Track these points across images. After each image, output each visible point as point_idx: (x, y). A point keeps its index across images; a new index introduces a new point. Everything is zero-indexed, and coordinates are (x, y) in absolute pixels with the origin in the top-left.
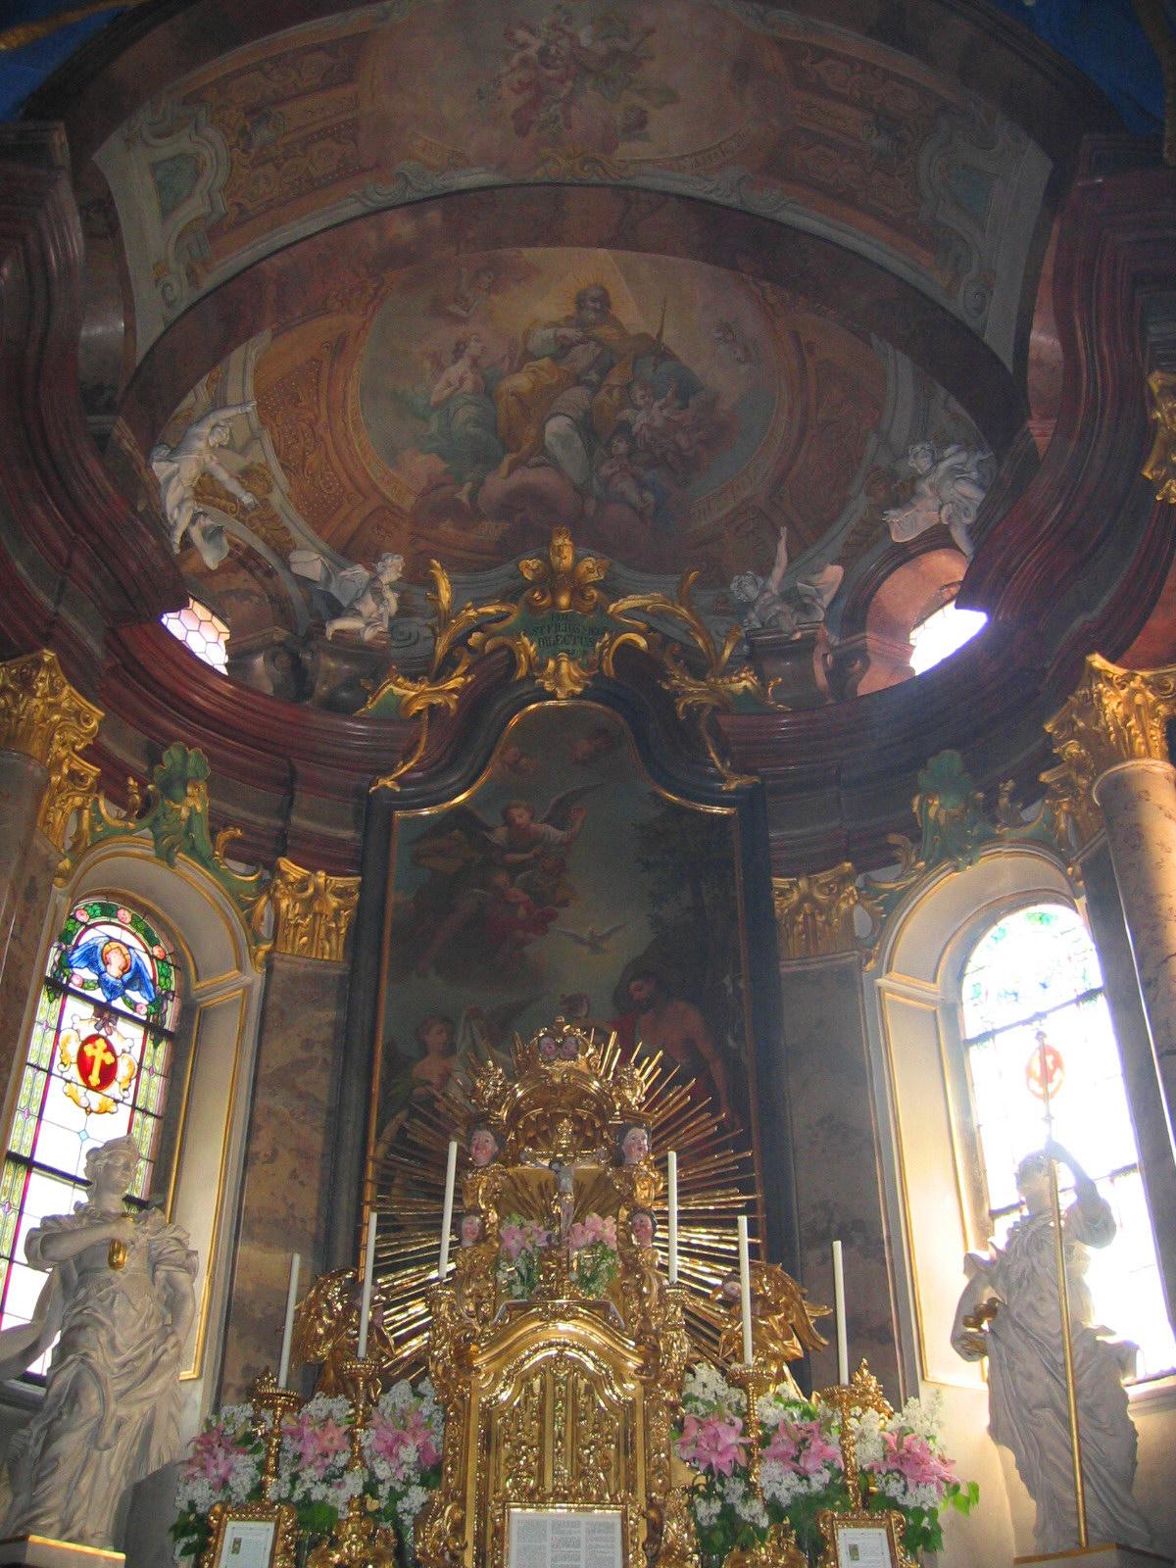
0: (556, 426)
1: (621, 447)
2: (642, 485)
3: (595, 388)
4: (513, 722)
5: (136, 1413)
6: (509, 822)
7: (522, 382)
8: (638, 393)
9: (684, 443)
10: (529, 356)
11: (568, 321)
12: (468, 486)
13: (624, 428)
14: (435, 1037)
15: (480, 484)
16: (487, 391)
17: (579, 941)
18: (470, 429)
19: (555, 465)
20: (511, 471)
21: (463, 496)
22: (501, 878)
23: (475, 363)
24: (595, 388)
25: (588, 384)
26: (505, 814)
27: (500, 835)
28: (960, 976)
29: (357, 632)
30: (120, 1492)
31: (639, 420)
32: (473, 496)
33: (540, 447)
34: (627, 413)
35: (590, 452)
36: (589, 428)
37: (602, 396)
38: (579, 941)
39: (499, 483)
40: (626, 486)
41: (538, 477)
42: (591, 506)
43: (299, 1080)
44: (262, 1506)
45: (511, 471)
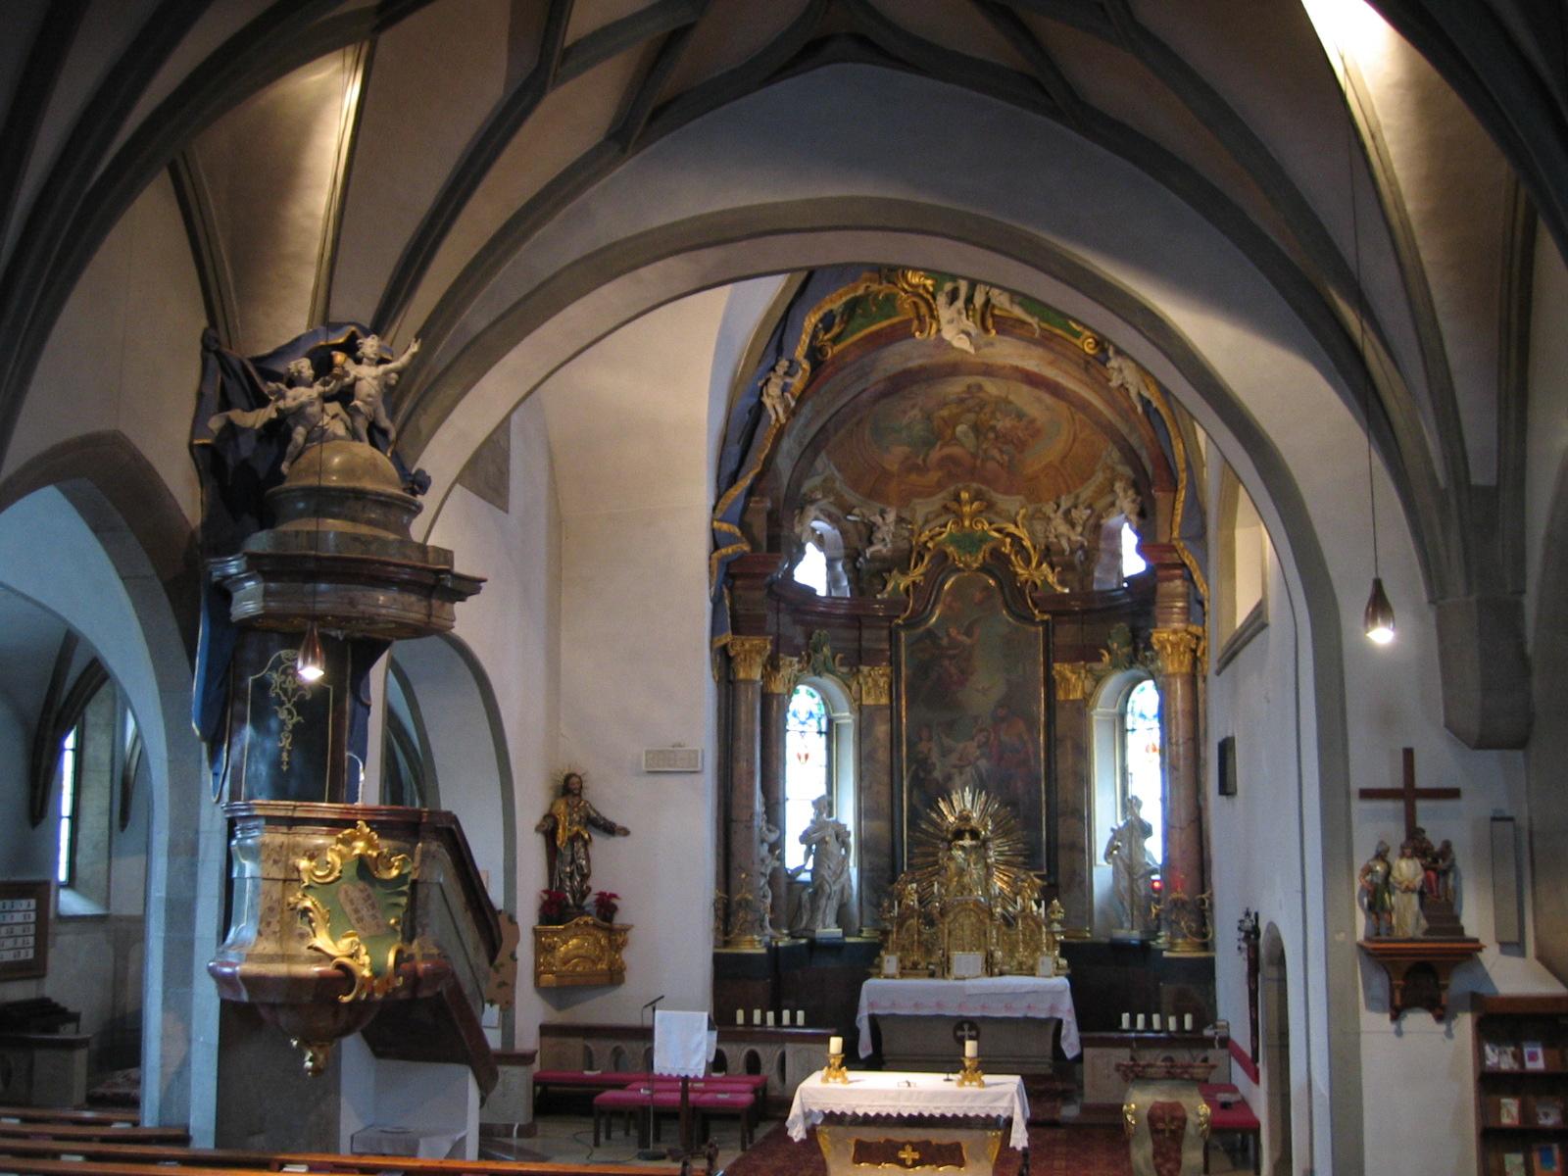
0: (961, 428)
1: (992, 435)
2: (1001, 451)
3: (978, 413)
4: (946, 587)
5: (836, 888)
6: (948, 635)
7: (945, 413)
8: (998, 415)
9: (1021, 435)
10: (946, 404)
11: (963, 392)
12: (921, 457)
13: (993, 428)
14: (925, 734)
15: (927, 455)
16: (928, 417)
17: (977, 690)
18: (922, 433)
19: (962, 446)
20: (941, 449)
21: (920, 461)
22: (946, 663)
23: (921, 409)
24: (978, 413)
25: (975, 412)
26: (947, 631)
27: (945, 642)
28: (1127, 702)
29: (880, 551)
30: (821, 911)
31: (1000, 425)
32: (924, 461)
33: (954, 437)
34: (993, 422)
35: (977, 438)
36: (977, 429)
37: (982, 415)
38: (977, 690)
39: (936, 454)
40: (995, 453)
41: (955, 450)
42: (979, 462)
43: (746, 548)
44: (575, 795)
45: (941, 449)
